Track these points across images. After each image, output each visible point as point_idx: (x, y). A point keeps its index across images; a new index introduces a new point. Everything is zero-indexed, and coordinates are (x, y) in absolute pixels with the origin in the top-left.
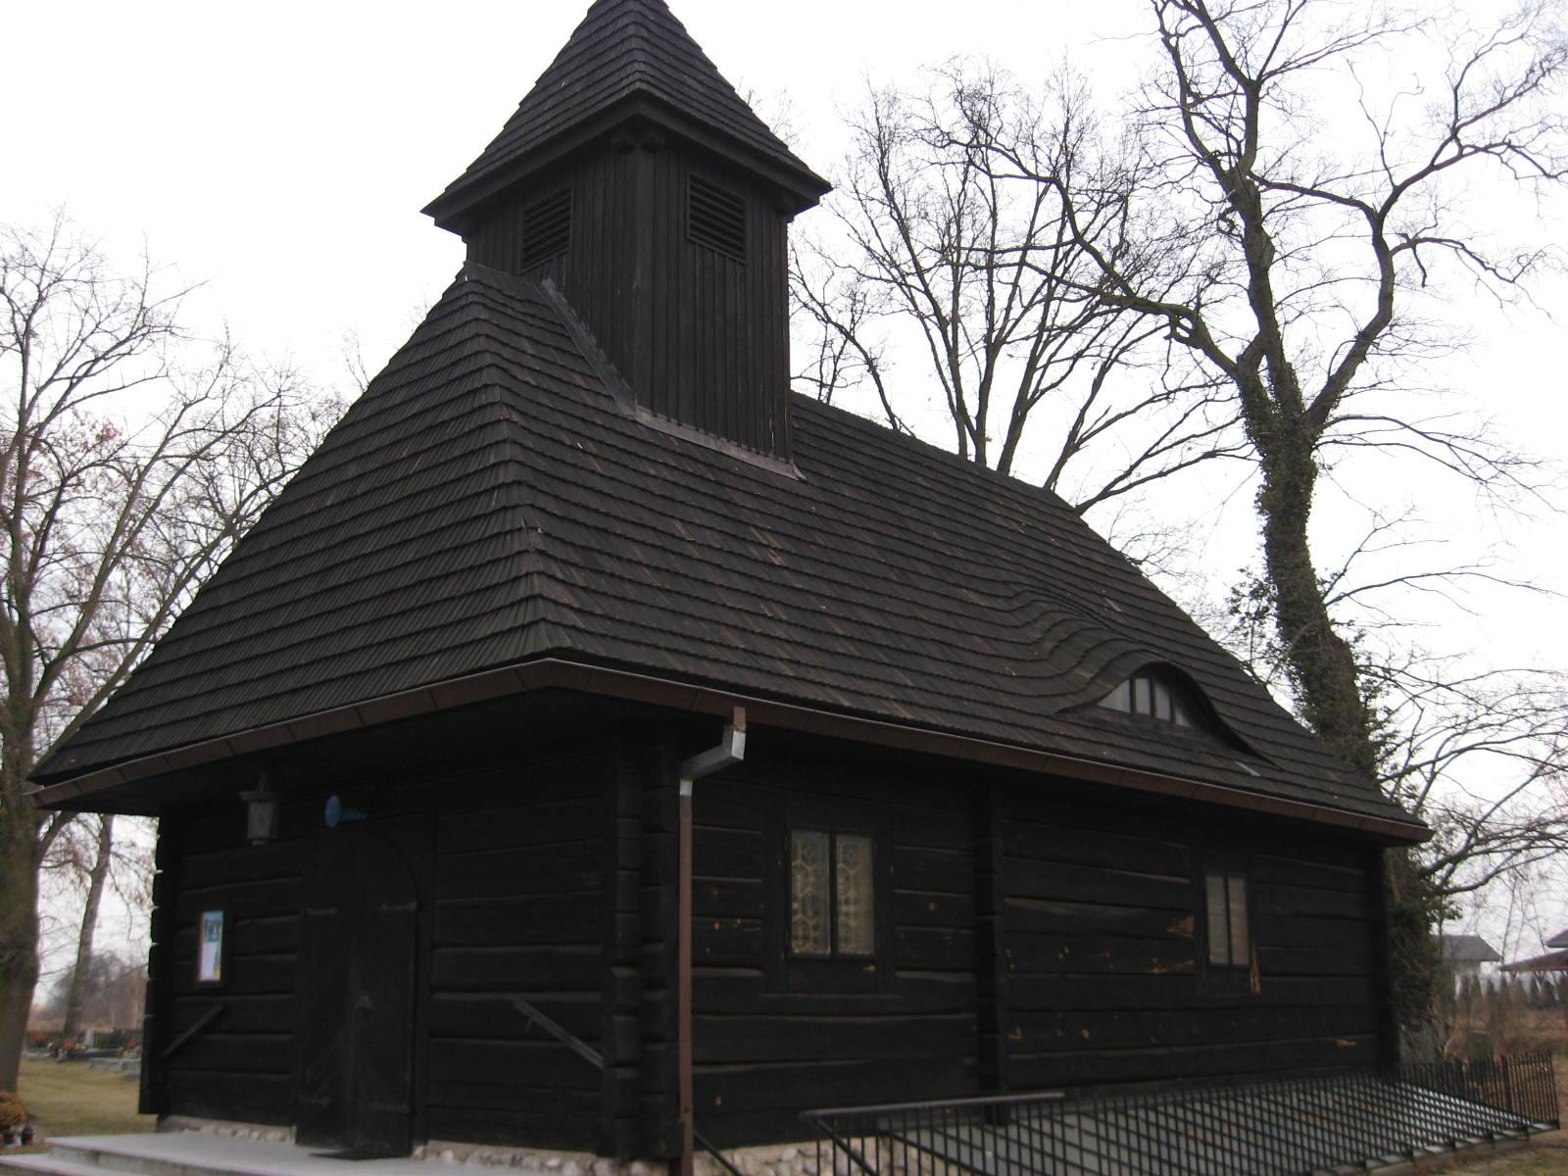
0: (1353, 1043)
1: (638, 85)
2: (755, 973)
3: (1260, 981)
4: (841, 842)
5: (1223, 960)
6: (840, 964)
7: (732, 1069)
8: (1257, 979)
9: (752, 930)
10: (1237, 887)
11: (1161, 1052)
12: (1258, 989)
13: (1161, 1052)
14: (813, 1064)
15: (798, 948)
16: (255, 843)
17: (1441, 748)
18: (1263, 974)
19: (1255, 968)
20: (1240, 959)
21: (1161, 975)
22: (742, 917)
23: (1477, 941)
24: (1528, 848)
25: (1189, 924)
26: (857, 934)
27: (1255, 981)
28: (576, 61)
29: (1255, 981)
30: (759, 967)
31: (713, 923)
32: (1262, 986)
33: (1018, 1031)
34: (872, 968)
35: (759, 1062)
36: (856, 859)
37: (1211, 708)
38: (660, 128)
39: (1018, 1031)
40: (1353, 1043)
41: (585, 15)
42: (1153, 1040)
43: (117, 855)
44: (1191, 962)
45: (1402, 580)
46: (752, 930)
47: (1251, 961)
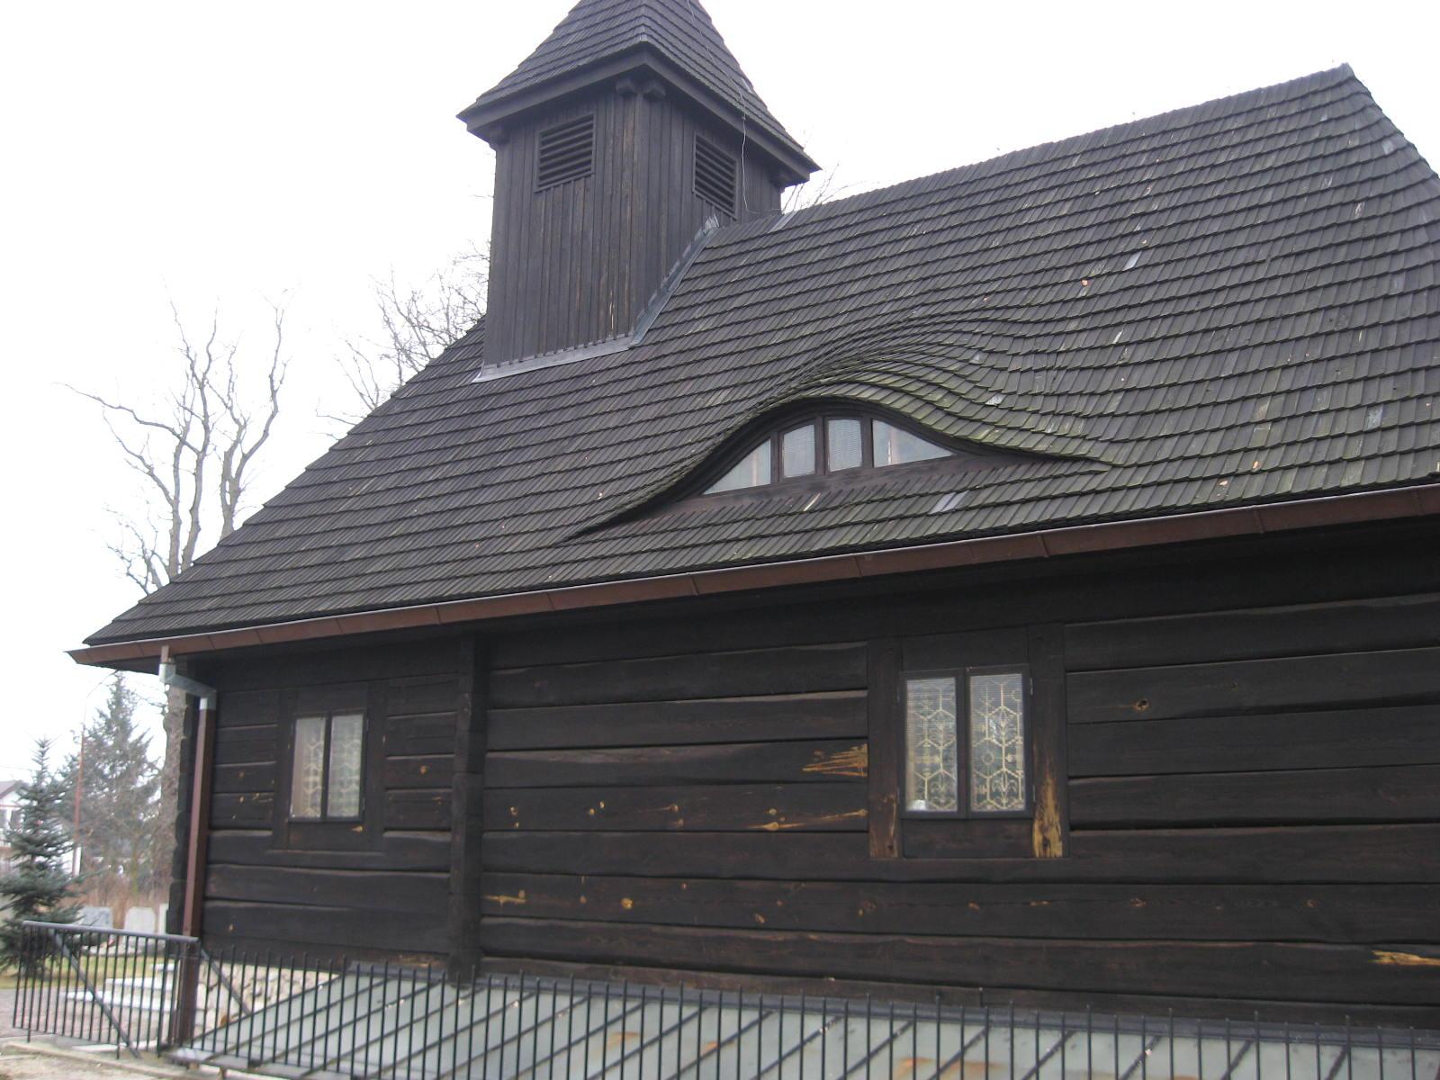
1: (645, 39)
2: (268, 833)
4: (978, 683)
5: (313, 813)
6: (329, 825)
7: (242, 905)
9: (266, 801)
14: (301, 907)
15: (1021, 807)
19: (1051, 814)
22: (260, 792)
25: (858, 758)
26: (347, 802)
27: (1049, 839)
30: (270, 829)
31: (239, 798)
32: (1068, 844)
33: (522, 894)
34: (360, 829)
35: (305, 904)
36: (350, 735)
37: (1020, 450)
38: (619, 77)
39: (522, 894)
41: (551, 32)
44: (862, 813)
45: (274, 393)
46: (266, 801)
47: (1033, 802)
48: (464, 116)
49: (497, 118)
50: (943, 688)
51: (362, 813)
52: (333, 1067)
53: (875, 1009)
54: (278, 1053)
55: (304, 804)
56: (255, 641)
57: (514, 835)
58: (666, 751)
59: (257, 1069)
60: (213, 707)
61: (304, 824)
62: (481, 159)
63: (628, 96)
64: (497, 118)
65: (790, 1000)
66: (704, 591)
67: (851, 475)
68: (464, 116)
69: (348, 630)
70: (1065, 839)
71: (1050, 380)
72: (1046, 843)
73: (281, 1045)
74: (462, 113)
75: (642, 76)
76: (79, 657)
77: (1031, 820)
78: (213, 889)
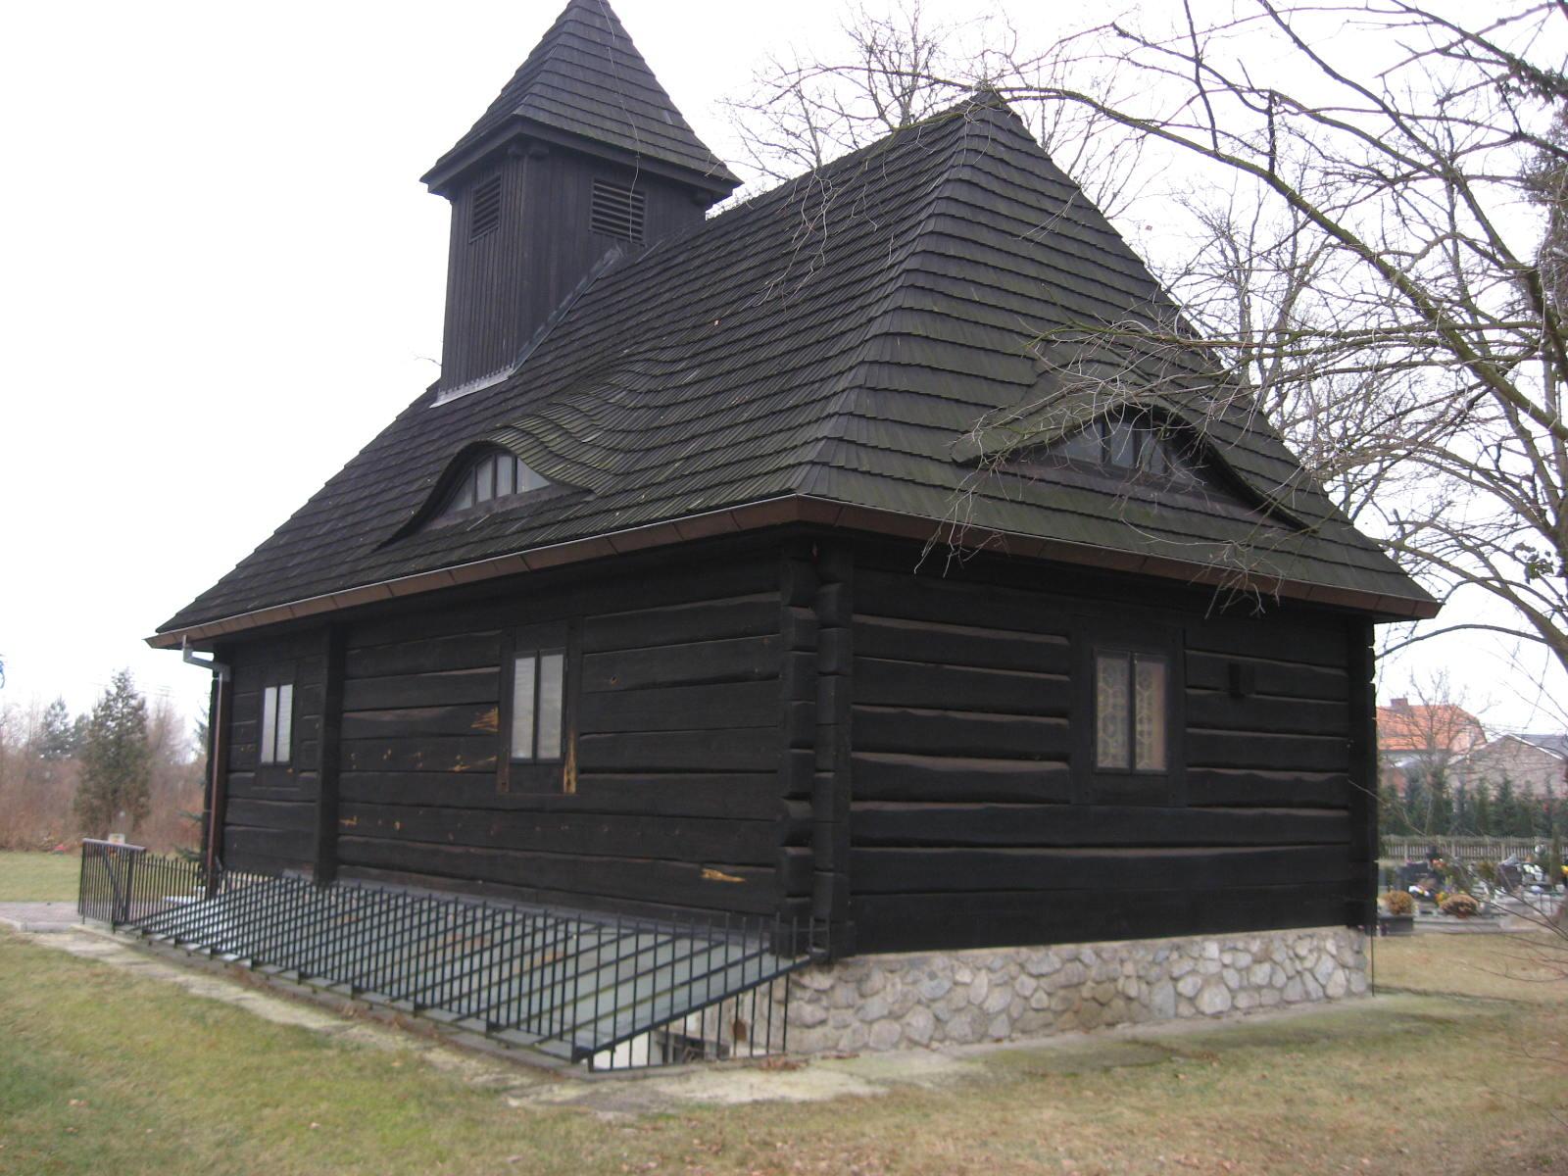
0: (737, 879)
3: (576, 779)
6: (276, 765)
8: (573, 776)
10: (554, 665)
11: (458, 850)
12: (573, 789)
13: (458, 850)
16: (209, 656)
17: (1329, 109)
18: (581, 771)
19: (572, 762)
20: (551, 749)
21: (461, 772)
23: (1454, 710)
24: (1325, 360)
25: (493, 716)
27: (570, 781)
28: (365, 503)
29: (570, 781)
40: (737, 879)
42: (451, 837)
43: (817, 153)
44: (493, 759)
48: (425, 179)
49: (446, 177)
50: (530, 662)
51: (291, 758)
52: (447, 1007)
53: (660, 929)
54: (565, 1027)
55: (267, 756)
56: (448, 582)
57: (353, 774)
58: (415, 712)
59: (494, 1034)
60: (228, 679)
61: (267, 766)
62: (442, 209)
63: (518, 158)
64: (446, 177)
65: (733, 938)
66: (621, 549)
67: (505, 499)
68: (425, 179)
69: (342, 605)
70: (578, 782)
71: (1479, 135)
72: (569, 783)
73: (456, 992)
74: (445, 164)
75: (522, 140)
76: (152, 642)
77: (563, 765)
78: (229, 818)
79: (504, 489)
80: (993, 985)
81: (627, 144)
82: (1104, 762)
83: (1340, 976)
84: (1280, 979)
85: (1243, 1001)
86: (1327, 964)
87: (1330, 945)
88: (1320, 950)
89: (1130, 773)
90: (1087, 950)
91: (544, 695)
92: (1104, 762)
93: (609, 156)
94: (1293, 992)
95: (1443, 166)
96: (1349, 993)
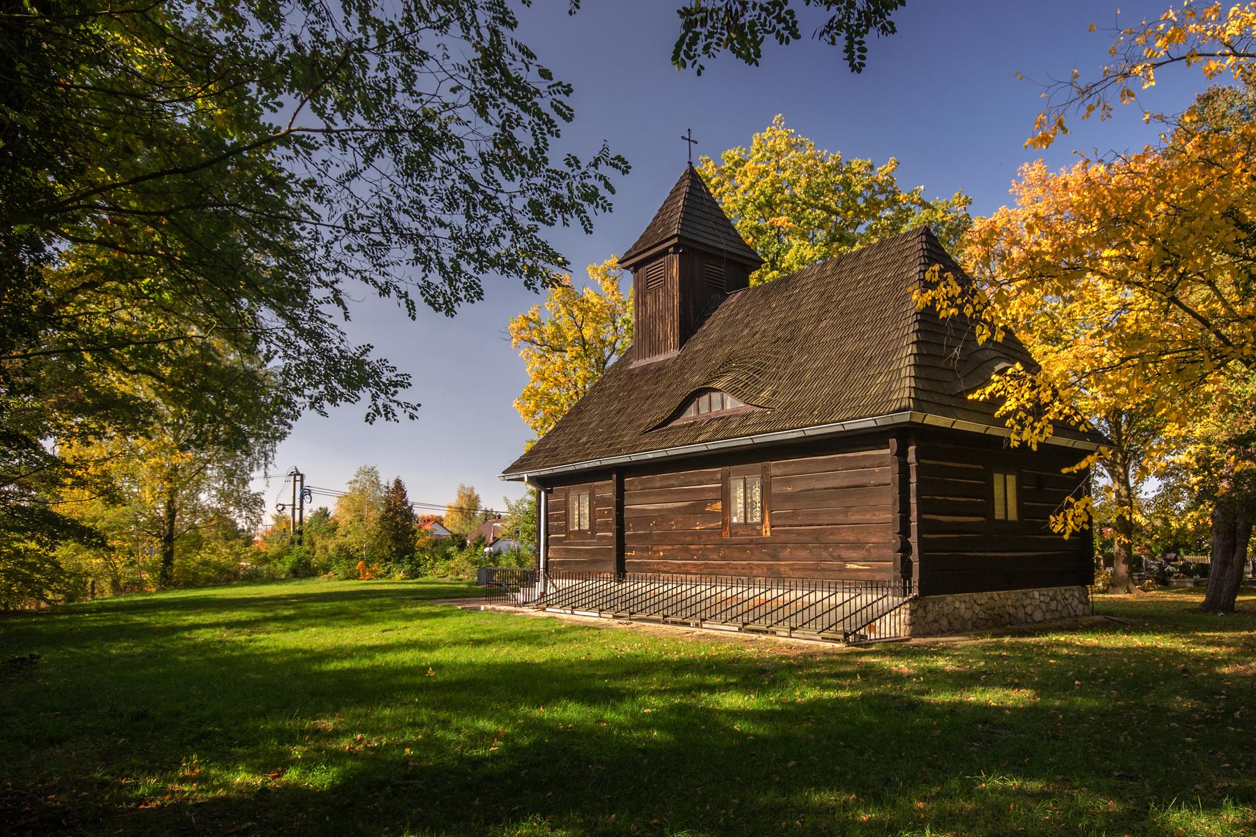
10: (1011, 479)
19: (767, 523)
25: (719, 505)
79: (716, 408)
80: (967, 609)
81: (720, 246)
82: (997, 517)
83: (1080, 606)
84: (1060, 607)
85: (1048, 617)
86: (1076, 602)
87: (1076, 594)
88: (1073, 595)
89: (1006, 521)
90: (995, 594)
91: (1002, 491)
92: (997, 517)
93: (711, 251)
94: (1065, 614)
95: (389, 85)
96: (1084, 614)
